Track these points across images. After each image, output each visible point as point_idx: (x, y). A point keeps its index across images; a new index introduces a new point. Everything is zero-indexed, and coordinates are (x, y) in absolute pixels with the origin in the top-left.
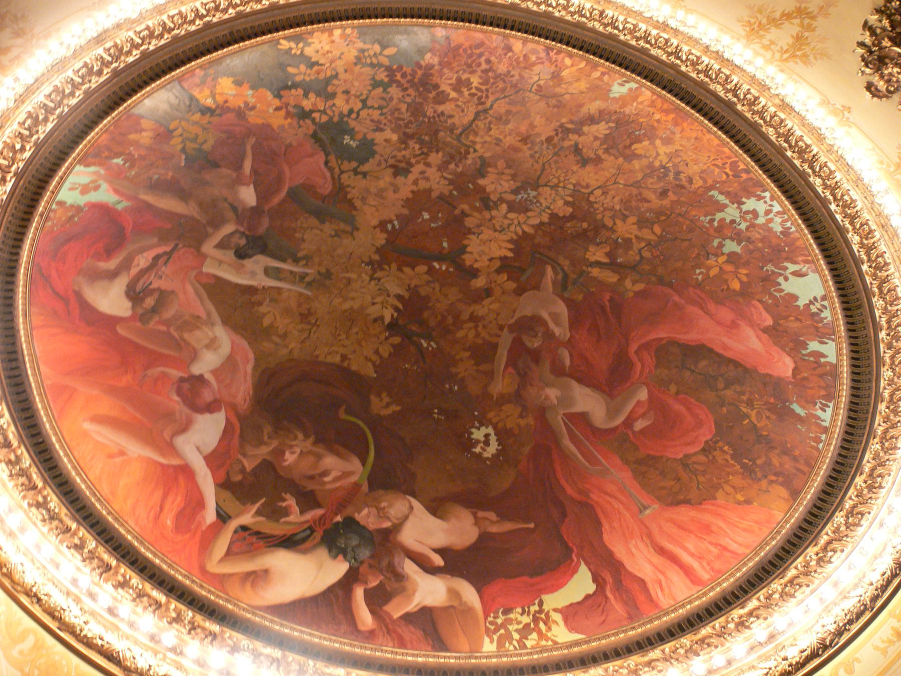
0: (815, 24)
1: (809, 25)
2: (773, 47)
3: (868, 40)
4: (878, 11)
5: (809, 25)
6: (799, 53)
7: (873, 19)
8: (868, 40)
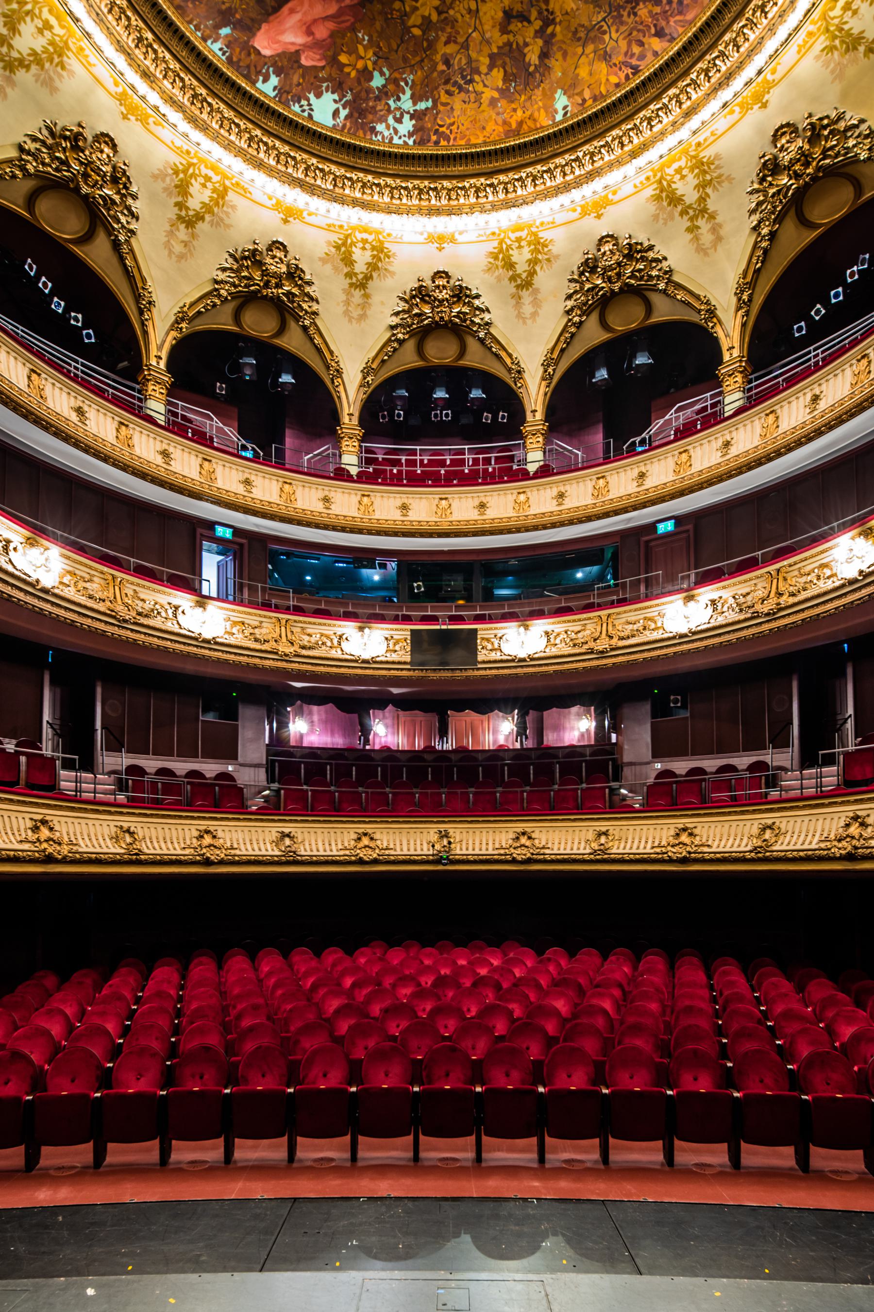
0: (513, 284)
1: (516, 281)
2: (678, 176)
3: (477, 302)
4: (315, 313)
5: (516, 281)
6: (664, 195)
7: (487, 317)
8: (477, 302)
